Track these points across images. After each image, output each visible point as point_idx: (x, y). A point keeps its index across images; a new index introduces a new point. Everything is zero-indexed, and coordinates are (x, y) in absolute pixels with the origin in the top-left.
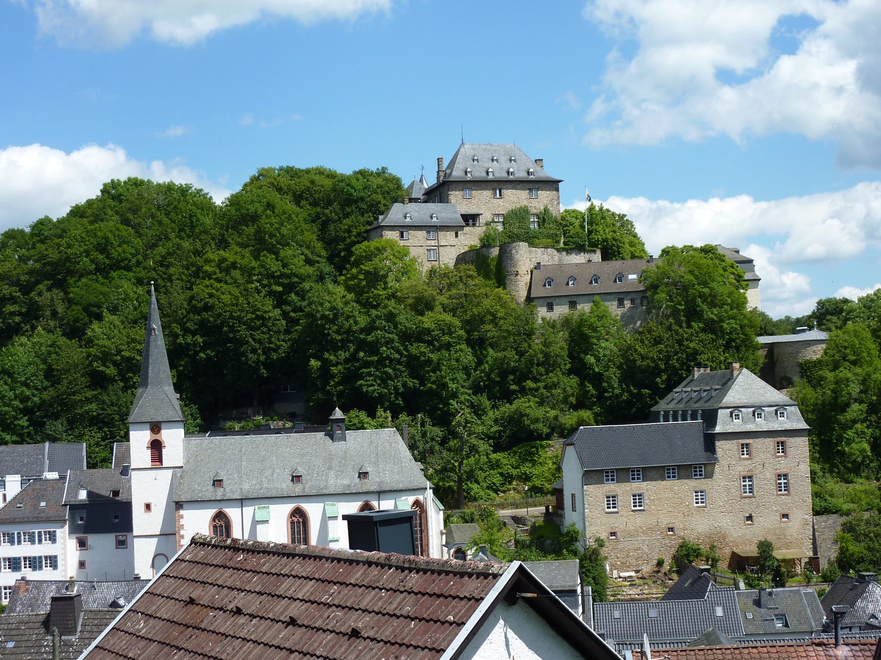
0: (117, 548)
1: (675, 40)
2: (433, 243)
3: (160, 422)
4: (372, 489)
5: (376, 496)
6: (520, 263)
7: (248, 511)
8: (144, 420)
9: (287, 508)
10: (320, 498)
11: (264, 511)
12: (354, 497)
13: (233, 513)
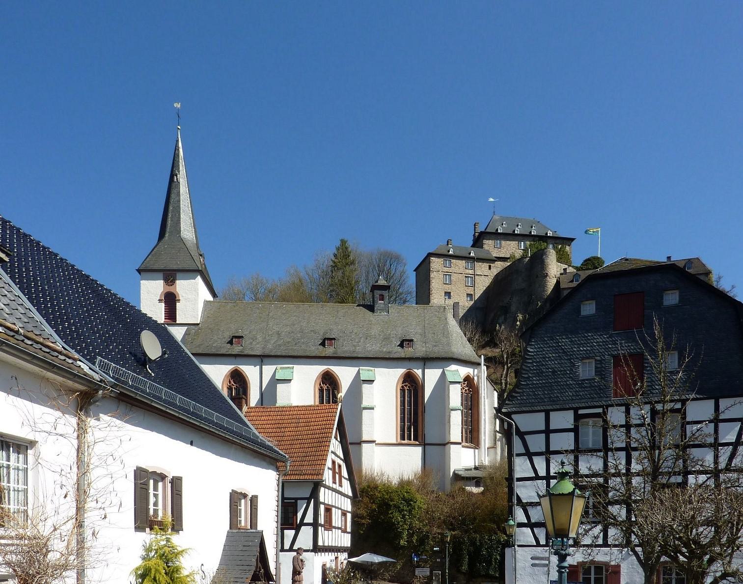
0: (182, 477)
1: (496, 459)
2: (471, 272)
3: (312, 551)
4: (418, 355)
5: (422, 364)
6: (550, 267)
7: (269, 370)
8: (156, 267)
9: (316, 370)
10: (354, 362)
11: (287, 372)
12: (395, 363)
13: (250, 372)
